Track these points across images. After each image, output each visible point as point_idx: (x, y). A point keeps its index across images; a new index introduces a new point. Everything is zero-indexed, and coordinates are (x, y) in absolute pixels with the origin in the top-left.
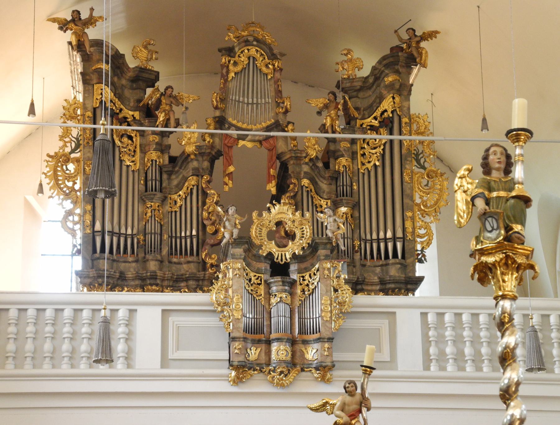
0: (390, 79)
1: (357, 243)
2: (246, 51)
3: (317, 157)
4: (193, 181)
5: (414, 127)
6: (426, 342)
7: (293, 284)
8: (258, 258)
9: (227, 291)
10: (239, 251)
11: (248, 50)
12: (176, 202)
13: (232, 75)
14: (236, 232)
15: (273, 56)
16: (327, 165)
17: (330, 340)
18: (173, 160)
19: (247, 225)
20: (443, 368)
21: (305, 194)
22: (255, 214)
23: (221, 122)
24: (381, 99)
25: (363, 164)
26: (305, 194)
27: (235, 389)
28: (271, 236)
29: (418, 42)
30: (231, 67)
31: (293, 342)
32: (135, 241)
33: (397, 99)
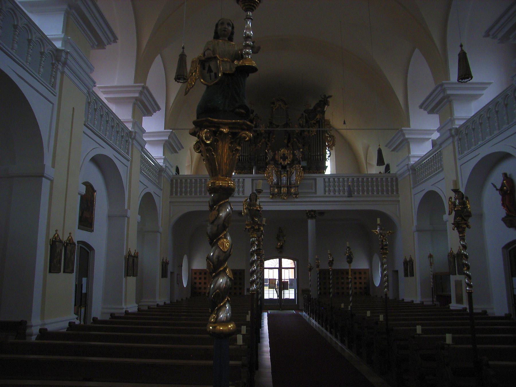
0: (319, 109)
1: (310, 156)
2: (278, 103)
3: (298, 133)
4: (263, 140)
5: (326, 123)
6: (325, 186)
7: (287, 171)
8: (278, 164)
9: (269, 173)
10: (272, 162)
11: (279, 103)
12: (259, 146)
13: (274, 110)
14: (271, 157)
15: (285, 104)
16: (301, 134)
17: (298, 187)
18: (258, 134)
19: (275, 155)
20: (329, 194)
21: (295, 143)
22: (277, 152)
23: (271, 123)
24: (317, 115)
25: (311, 134)
26: (295, 143)
27: (272, 200)
28: (281, 158)
29: (327, 99)
30: (274, 108)
31: (288, 187)
32: (248, 157)
33: (321, 115)
